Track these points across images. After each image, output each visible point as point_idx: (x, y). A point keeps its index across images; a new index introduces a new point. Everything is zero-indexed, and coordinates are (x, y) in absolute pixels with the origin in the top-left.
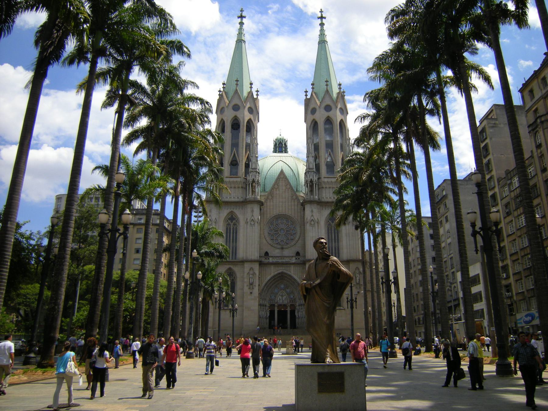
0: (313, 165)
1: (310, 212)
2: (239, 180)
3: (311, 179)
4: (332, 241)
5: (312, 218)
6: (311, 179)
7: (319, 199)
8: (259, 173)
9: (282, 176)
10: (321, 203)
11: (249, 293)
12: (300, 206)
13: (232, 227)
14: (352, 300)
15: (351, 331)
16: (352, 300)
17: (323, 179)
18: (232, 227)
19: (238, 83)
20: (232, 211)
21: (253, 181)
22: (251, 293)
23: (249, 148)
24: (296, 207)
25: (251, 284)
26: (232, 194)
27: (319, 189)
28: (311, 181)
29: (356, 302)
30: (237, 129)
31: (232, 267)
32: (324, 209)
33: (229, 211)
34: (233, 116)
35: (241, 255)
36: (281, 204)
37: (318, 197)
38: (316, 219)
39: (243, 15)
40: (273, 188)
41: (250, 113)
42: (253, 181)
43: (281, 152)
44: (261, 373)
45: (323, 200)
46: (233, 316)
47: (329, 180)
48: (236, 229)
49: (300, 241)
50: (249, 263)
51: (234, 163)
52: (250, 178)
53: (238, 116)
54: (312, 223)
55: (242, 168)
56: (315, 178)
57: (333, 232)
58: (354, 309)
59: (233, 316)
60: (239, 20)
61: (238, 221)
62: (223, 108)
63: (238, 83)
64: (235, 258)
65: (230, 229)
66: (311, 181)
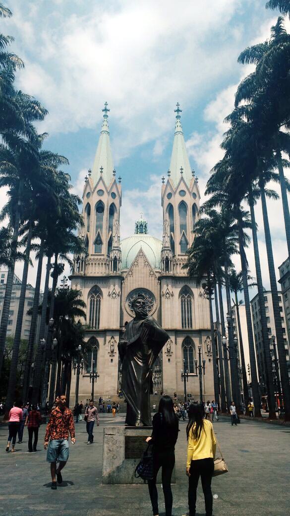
0: (168, 245)
1: (167, 287)
2: (102, 257)
3: (167, 256)
4: (185, 313)
5: (168, 291)
6: (167, 256)
7: (85, 274)
8: (120, 251)
9: (141, 254)
10: (175, 279)
11: (110, 360)
12: (157, 281)
13: (95, 300)
14: (200, 366)
15: (199, 397)
16: (200, 366)
17: (177, 257)
18: (95, 300)
19: (183, 171)
20: (186, 286)
21: (115, 258)
22: (112, 360)
23: (112, 229)
24: (153, 282)
25: (112, 352)
26: (95, 271)
27: (174, 265)
28: (167, 258)
29: (204, 368)
30: (101, 212)
31: (95, 336)
32: (178, 283)
33: (94, 284)
34: (98, 200)
35: (103, 326)
36: (140, 278)
37: (84, 272)
38: (171, 292)
39: (108, 108)
40: (133, 265)
41: (112, 197)
42: (115, 258)
43: (142, 232)
44: (17, 440)
45: (177, 275)
46: (93, 382)
47: (96, 257)
48: (100, 301)
49: (156, 312)
50: (111, 333)
51: (98, 242)
52: (112, 255)
53: (103, 200)
54: (114, 296)
55: (104, 247)
56: (170, 255)
57: (186, 304)
58: (95, 383)
59: (93, 382)
60: (104, 113)
61: (101, 293)
62: (89, 193)
63: (183, 171)
64: (98, 328)
65: (94, 301)
66: (167, 258)
